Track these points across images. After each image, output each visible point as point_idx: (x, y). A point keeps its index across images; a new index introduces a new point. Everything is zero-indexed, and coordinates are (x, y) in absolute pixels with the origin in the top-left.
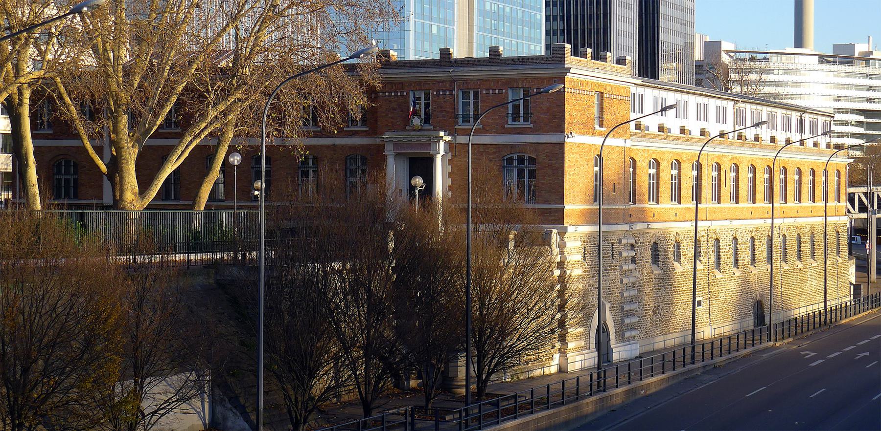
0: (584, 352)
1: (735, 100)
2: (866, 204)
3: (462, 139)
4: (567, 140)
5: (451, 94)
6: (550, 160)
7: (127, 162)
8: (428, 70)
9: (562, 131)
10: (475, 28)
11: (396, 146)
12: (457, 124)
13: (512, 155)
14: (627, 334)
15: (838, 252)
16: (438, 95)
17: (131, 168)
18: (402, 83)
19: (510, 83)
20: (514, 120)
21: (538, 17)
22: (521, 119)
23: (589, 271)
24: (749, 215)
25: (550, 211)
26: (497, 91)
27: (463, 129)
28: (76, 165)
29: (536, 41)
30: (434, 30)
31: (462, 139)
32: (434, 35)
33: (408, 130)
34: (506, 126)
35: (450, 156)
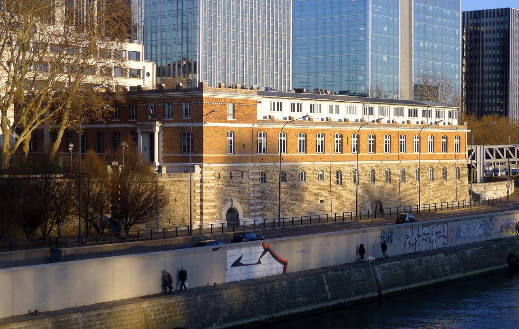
0: (216, 221)
1: (363, 103)
2: (510, 151)
3: (167, 125)
4: (204, 125)
5: (163, 105)
6: (198, 134)
7: (5, 136)
8: (155, 94)
9: (201, 121)
10: (413, 57)
11: (142, 128)
12: (165, 118)
13: (184, 132)
14: (251, 214)
15: (459, 177)
16: (158, 105)
17: (7, 139)
18: (145, 100)
19: (184, 100)
20: (169, 117)
21: (457, 49)
22: (135, 118)
23: (223, 184)
24: (386, 159)
25: (197, 157)
26: (179, 103)
27: (167, 121)
28: (119, 133)
29: (456, 62)
30: (385, 59)
31: (167, 125)
32: (385, 61)
33: (148, 121)
34: (182, 119)
35: (162, 132)
